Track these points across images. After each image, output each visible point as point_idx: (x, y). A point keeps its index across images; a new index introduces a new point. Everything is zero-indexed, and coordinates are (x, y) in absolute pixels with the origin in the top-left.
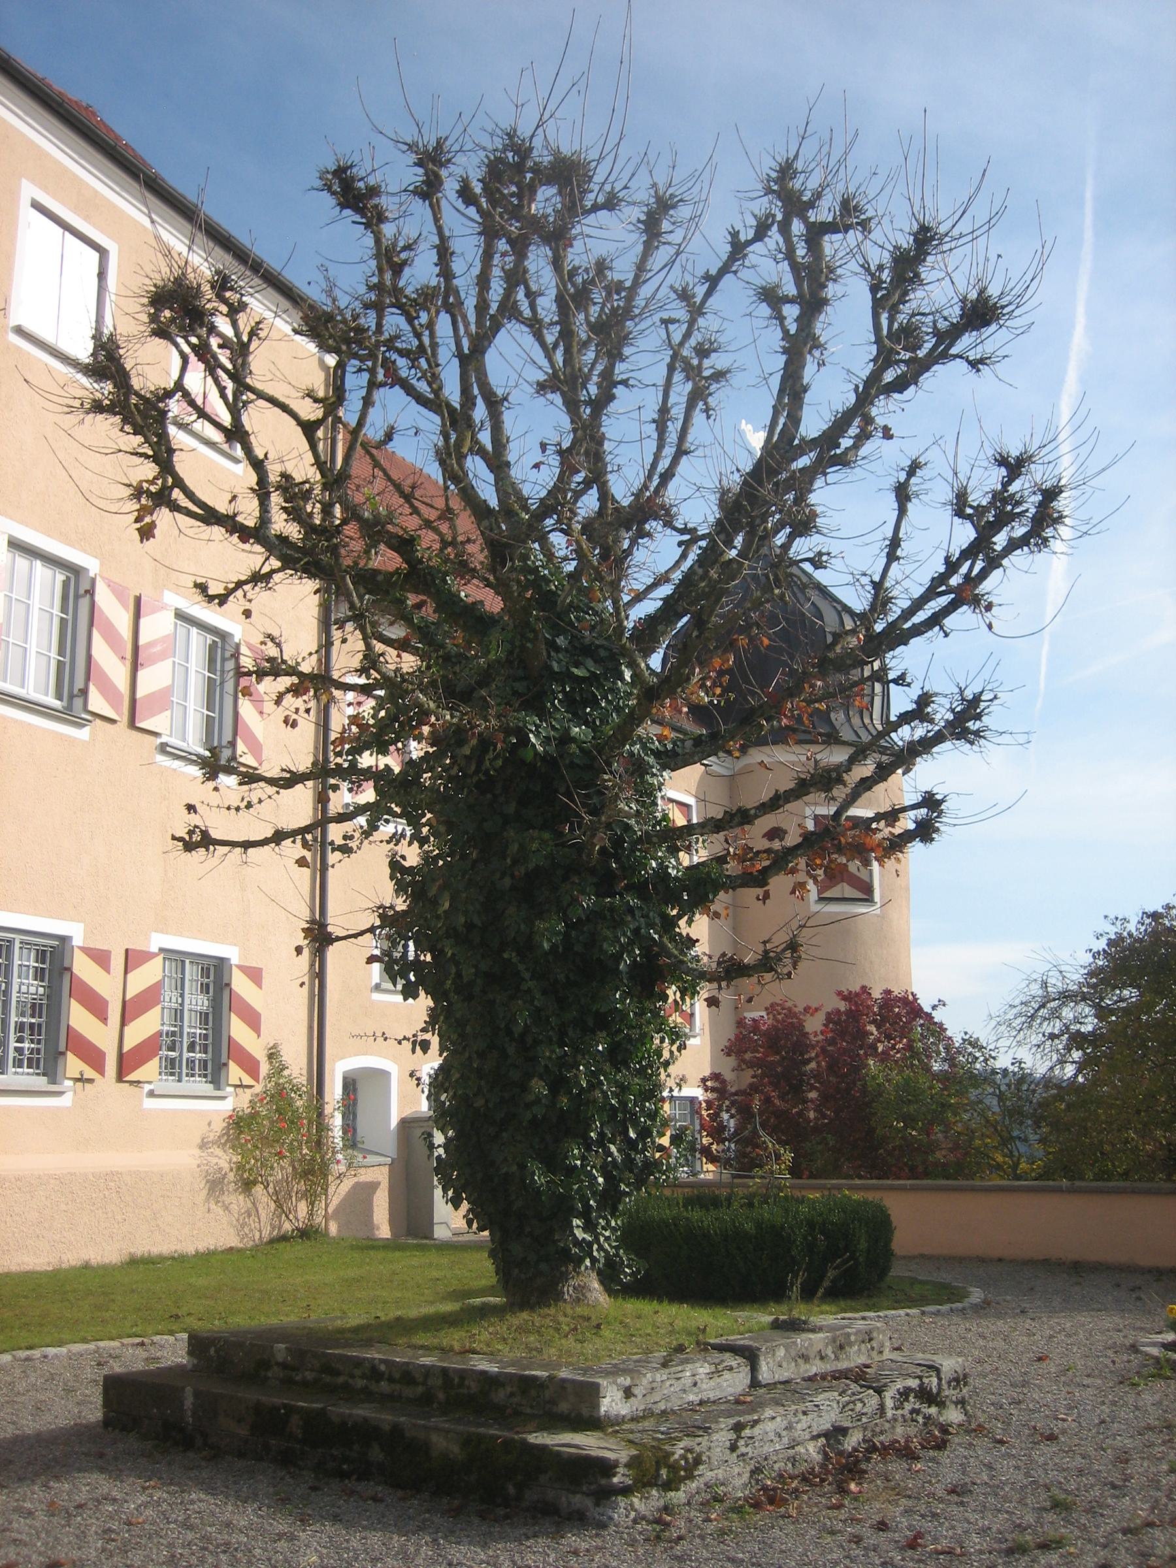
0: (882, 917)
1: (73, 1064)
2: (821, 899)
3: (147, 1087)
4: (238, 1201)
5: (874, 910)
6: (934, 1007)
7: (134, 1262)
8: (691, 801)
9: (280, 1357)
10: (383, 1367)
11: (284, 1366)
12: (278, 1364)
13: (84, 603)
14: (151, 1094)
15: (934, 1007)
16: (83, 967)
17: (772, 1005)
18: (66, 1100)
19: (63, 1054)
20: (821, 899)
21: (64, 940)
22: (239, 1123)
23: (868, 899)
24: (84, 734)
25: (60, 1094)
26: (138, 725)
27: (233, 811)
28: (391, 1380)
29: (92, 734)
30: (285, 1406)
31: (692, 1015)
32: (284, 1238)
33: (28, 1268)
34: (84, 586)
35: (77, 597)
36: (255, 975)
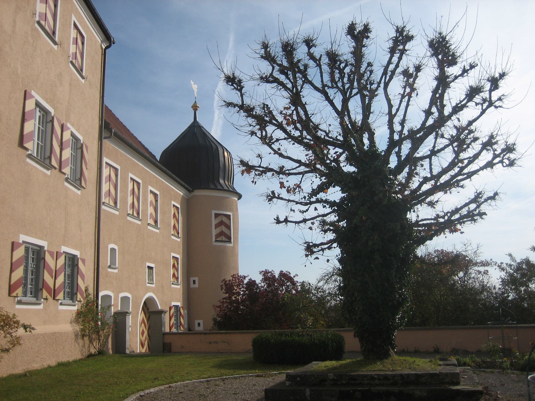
0: (233, 247)
1: (45, 294)
2: (216, 241)
3: (60, 301)
4: (81, 341)
5: (231, 245)
6: (294, 277)
7: (60, 365)
8: (179, 206)
9: (331, 378)
10: (376, 376)
11: (333, 380)
12: (330, 380)
13: (49, 125)
14: (61, 304)
15: (294, 277)
16: (48, 258)
17: (234, 275)
18: (41, 307)
19: (41, 289)
20: (216, 241)
21: (41, 247)
22: (79, 313)
23: (230, 241)
24: (48, 173)
25: (40, 304)
26: (63, 171)
27: (282, 219)
28: (379, 379)
29: (51, 173)
30: (352, 390)
31: (178, 278)
32: (90, 356)
33: (35, 368)
34: (49, 119)
35: (47, 122)
36: (83, 261)
